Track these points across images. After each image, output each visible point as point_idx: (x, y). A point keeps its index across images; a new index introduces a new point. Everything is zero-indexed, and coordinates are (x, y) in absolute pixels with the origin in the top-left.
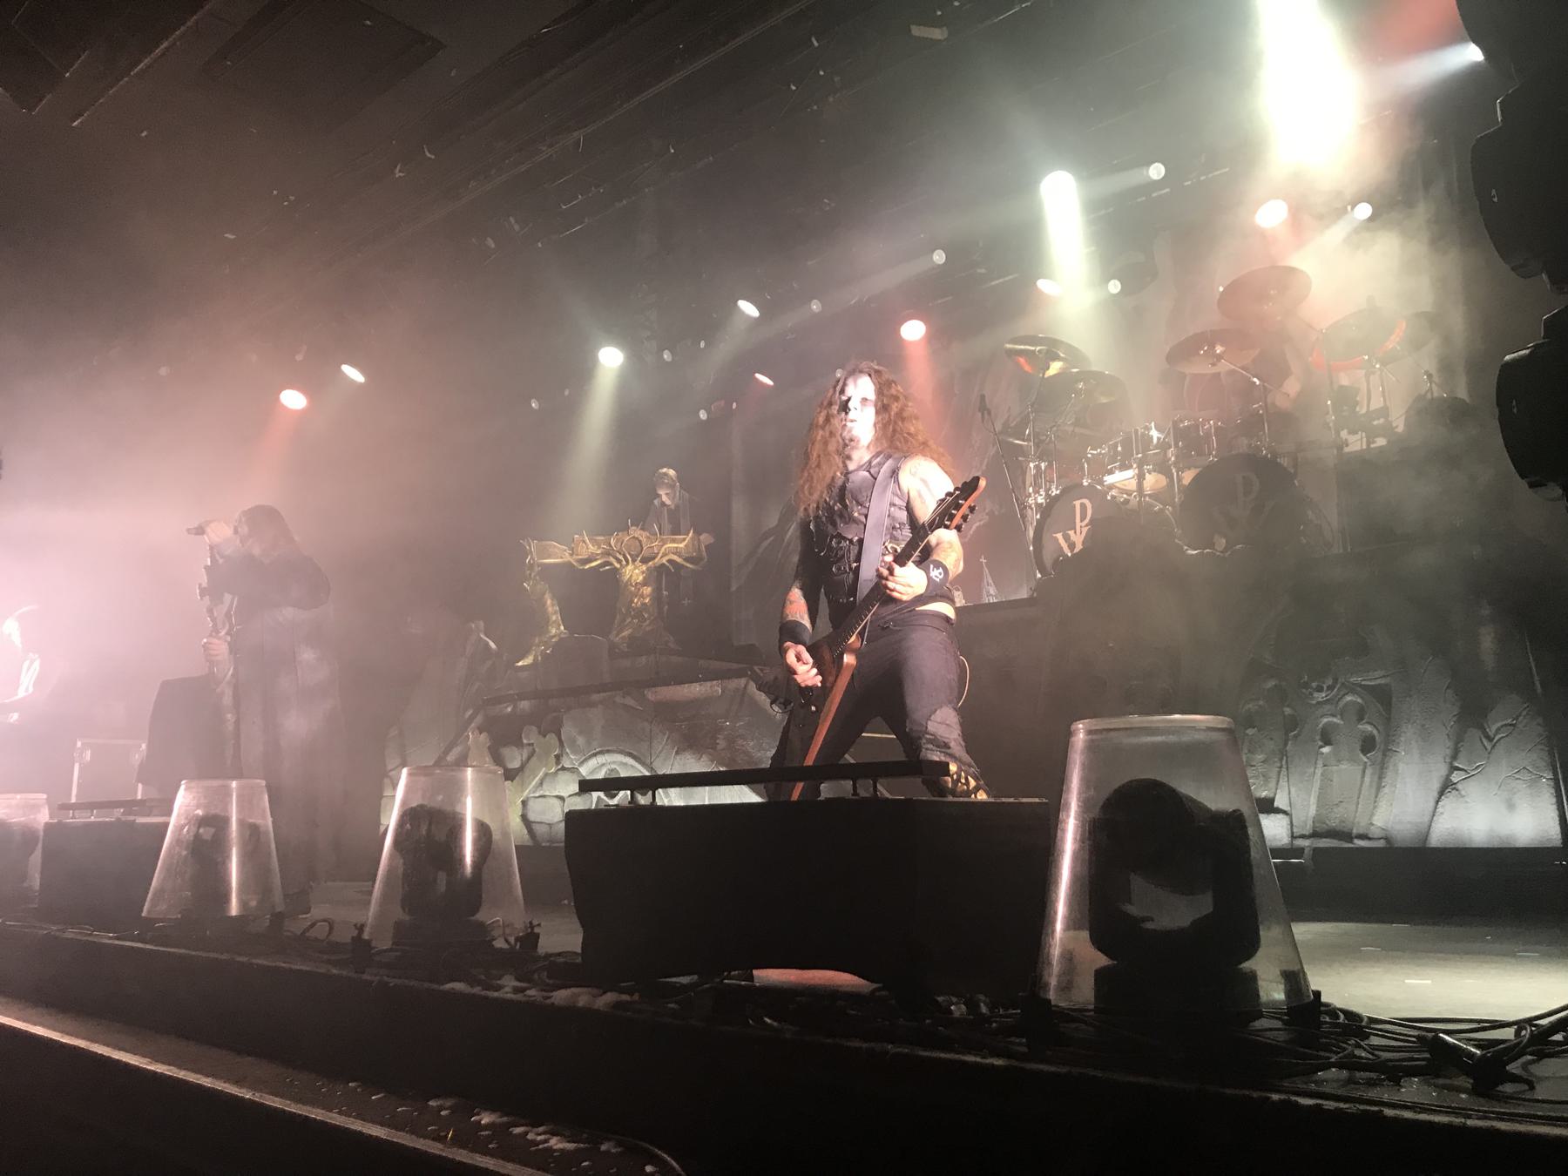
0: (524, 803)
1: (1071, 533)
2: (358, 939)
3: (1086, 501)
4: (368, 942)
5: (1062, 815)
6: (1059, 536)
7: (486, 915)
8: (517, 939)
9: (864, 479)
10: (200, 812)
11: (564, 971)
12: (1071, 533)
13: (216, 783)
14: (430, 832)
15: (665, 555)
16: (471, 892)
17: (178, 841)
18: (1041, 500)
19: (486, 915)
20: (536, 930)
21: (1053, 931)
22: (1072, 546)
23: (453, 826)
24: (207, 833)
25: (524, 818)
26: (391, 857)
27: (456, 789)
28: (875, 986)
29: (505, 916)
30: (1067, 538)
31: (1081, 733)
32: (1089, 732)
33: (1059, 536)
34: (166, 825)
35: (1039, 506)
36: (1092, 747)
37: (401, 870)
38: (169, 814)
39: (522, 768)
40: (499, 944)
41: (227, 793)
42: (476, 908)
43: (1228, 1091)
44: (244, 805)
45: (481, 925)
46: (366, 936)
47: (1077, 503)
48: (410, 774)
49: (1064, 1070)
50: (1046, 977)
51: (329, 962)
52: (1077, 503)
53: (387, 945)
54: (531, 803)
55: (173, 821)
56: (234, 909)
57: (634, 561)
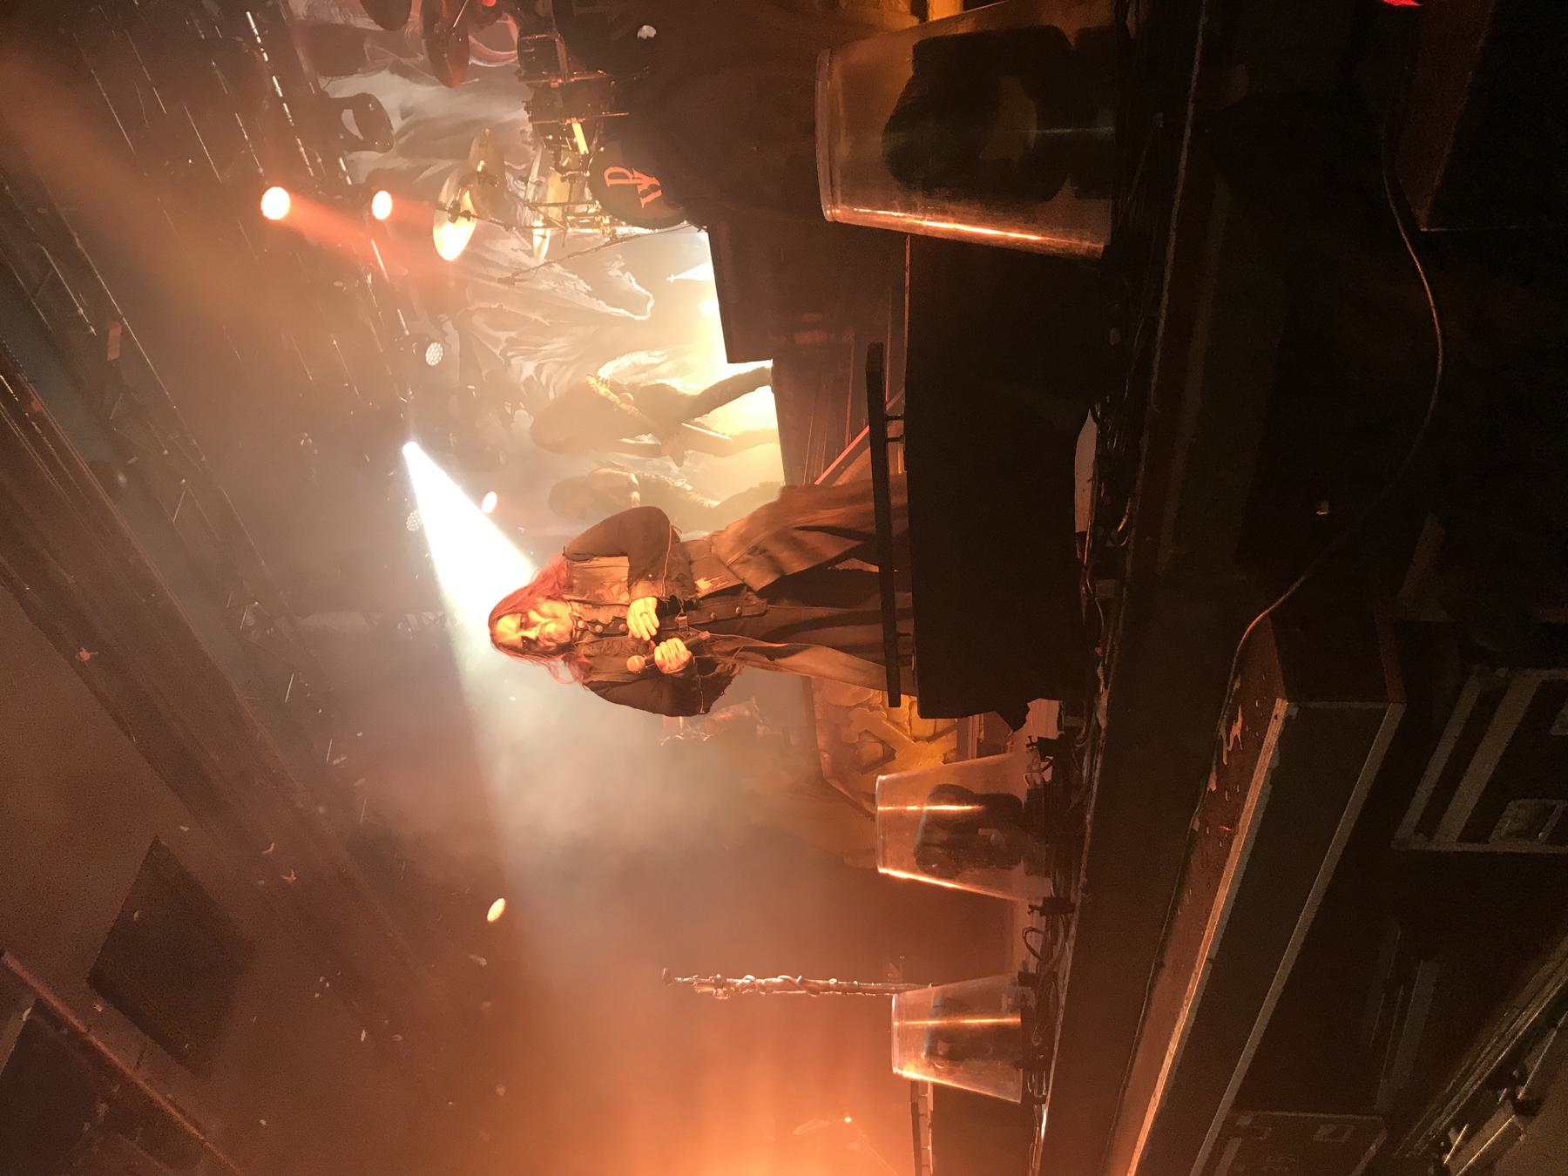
0: (916, 739)
1: (640, 189)
2: (1042, 912)
3: (607, 173)
4: (1046, 900)
5: (919, 232)
6: (644, 201)
7: (1021, 791)
8: (1043, 759)
9: (547, 607)
10: (923, 1055)
11: (1076, 705)
12: (640, 189)
13: (896, 1040)
14: (947, 844)
16: (998, 806)
17: (950, 1074)
18: (606, 221)
19: (1021, 791)
20: (1035, 740)
21: (1036, 242)
22: (653, 188)
23: (937, 821)
24: (942, 1048)
25: (929, 740)
26: (962, 882)
27: (898, 822)
28: (1090, 418)
29: (1021, 773)
30: (645, 194)
31: (835, 212)
32: (834, 204)
33: (644, 201)
34: (936, 1087)
35: (612, 223)
36: (851, 199)
37: (977, 872)
38: (925, 1084)
39: (882, 742)
40: (1048, 775)
41: (904, 1032)
42: (1011, 800)
43: (1297, 584)
44: (914, 1009)
45: (1030, 794)
46: (1040, 904)
47: (609, 182)
48: (884, 866)
49: (1173, 235)
50: (1082, 252)
51: (1066, 937)
52: (609, 182)
53: (1049, 883)
54: (916, 733)
55: (930, 1079)
56: (1013, 1020)
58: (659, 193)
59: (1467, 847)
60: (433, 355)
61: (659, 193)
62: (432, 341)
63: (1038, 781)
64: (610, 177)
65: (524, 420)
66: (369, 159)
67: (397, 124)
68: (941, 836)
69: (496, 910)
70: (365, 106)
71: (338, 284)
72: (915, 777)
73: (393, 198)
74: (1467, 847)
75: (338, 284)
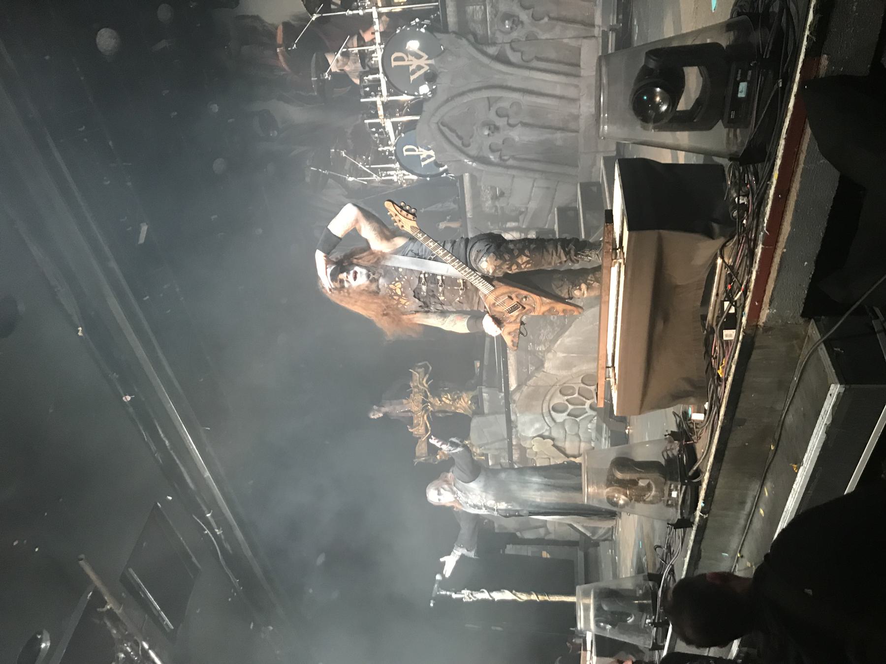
1: (422, 157)
6: (423, 164)
12: (422, 157)
47: (405, 153)
52: (405, 153)
59: (695, 468)
63: (671, 456)
68: (571, 214)
74: (695, 468)
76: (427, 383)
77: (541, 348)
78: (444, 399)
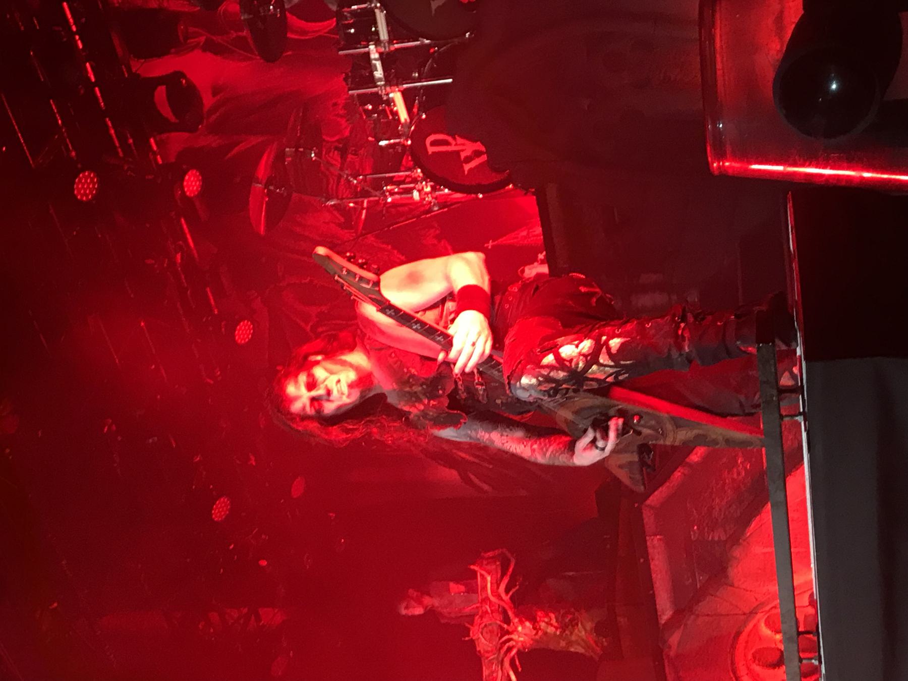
1: (463, 155)
3: (428, 141)
12: (463, 155)
15: (499, 597)
22: (477, 154)
33: (467, 167)
47: (431, 150)
52: (431, 150)
57: (508, 633)
58: (484, 158)
60: (243, 333)
61: (484, 158)
62: (243, 319)
64: (433, 143)
65: (336, 381)
66: (178, 141)
67: (208, 101)
69: (298, 488)
70: (183, 94)
71: (150, 261)
72: (664, 669)
73: (289, 407)
75: (150, 261)
76: (507, 591)
77: (718, 535)
78: (543, 625)
